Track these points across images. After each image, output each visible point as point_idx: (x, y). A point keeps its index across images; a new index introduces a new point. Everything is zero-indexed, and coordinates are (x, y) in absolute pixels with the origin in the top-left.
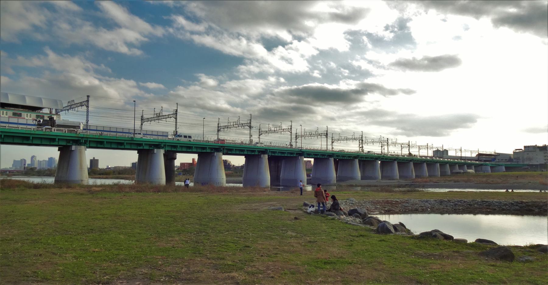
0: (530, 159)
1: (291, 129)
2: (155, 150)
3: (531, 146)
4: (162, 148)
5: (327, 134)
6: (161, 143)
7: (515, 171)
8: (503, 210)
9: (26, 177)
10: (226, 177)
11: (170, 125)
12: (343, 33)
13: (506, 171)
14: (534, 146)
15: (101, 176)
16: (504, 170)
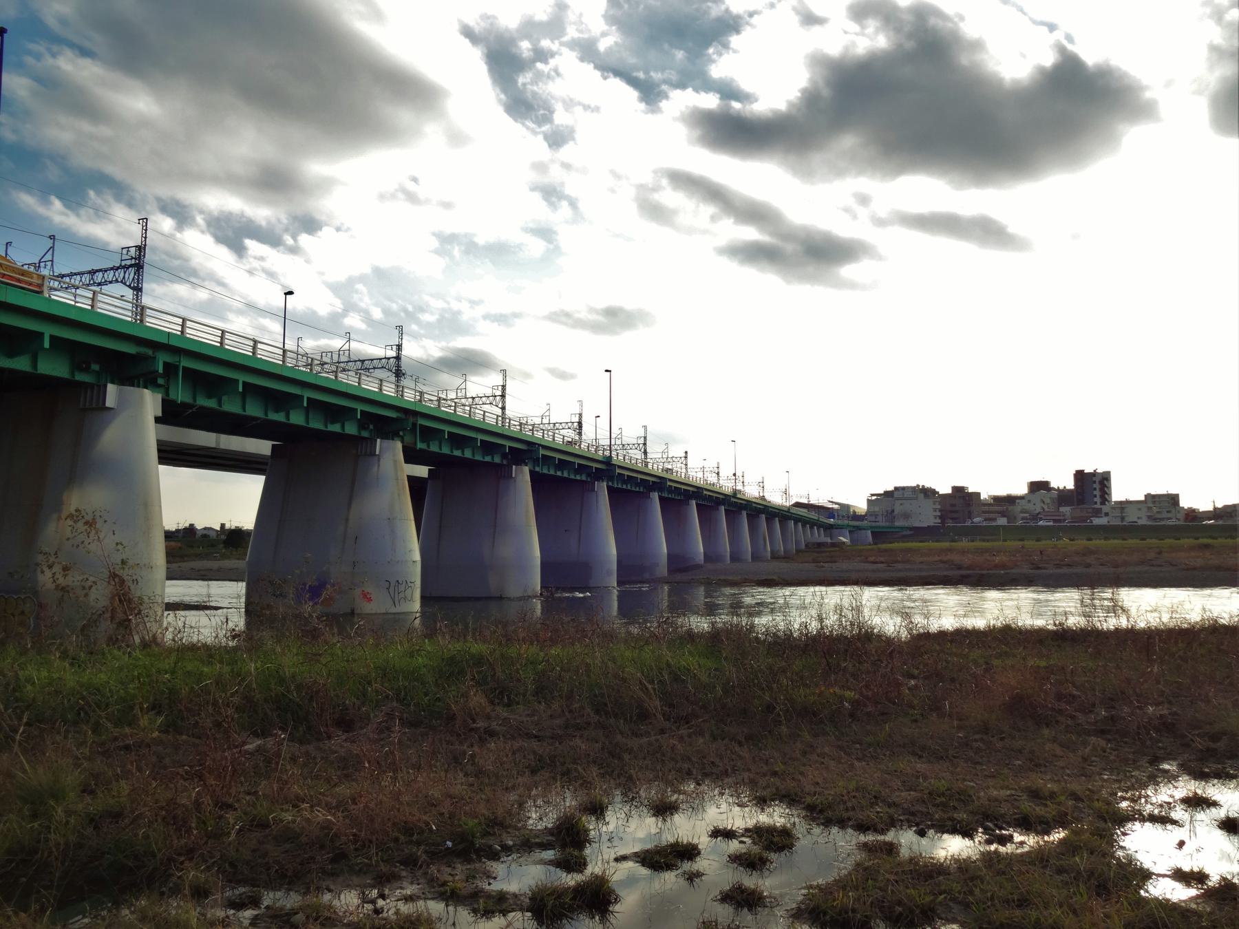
0: (906, 516)
1: (503, 396)
2: (111, 389)
3: (908, 487)
4: (149, 381)
5: (580, 424)
6: (150, 352)
7: (912, 542)
8: (1041, 642)
9: (939, 588)
10: (168, 562)
11: (116, 310)
12: (1069, 32)
13: (875, 544)
14: (914, 488)
15: (241, 458)
16: (870, 539)
